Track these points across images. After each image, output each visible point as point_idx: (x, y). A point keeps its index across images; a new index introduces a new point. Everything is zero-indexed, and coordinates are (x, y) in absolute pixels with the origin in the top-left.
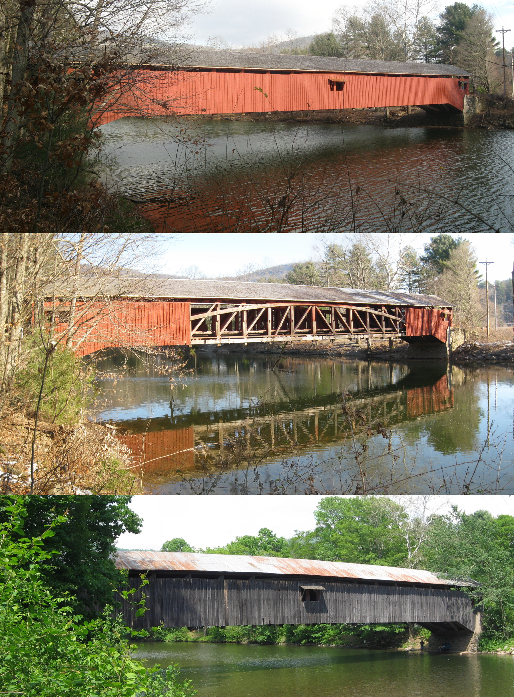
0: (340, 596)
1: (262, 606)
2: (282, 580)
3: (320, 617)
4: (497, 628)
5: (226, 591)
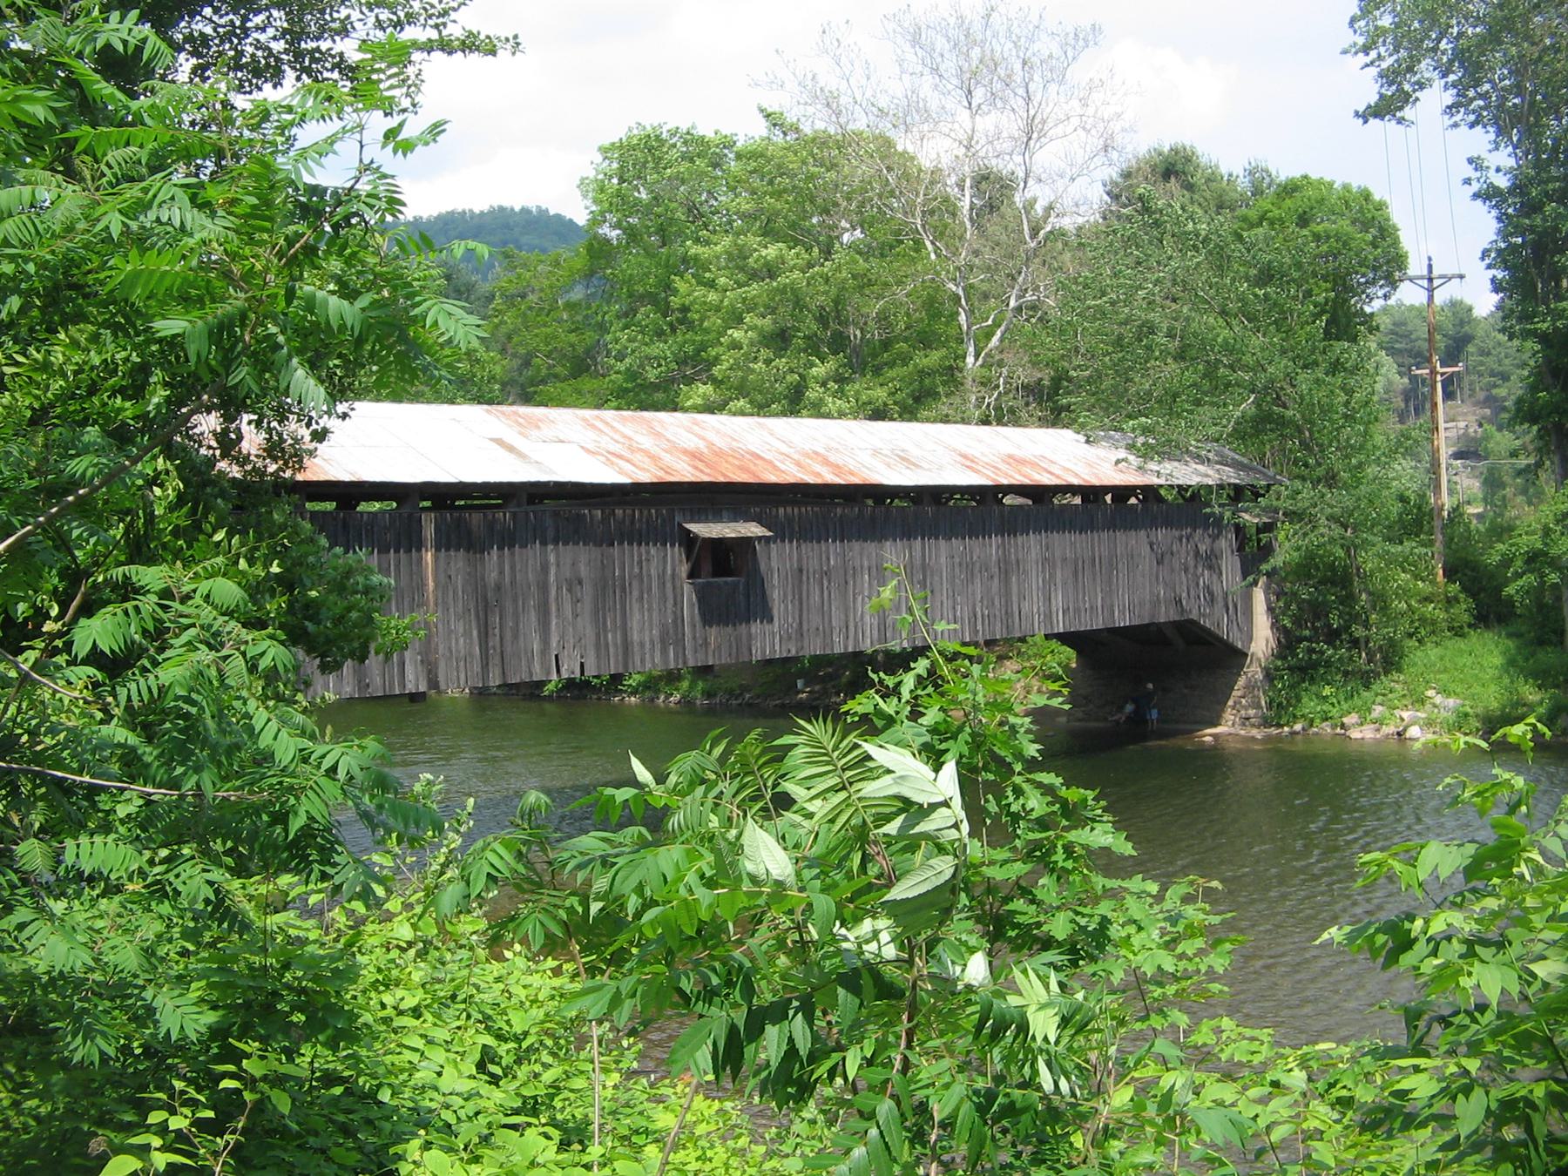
0: (813, 554)
1: (553, 608)
2: (621, 504)
3: (750, 635)
4: (1332, 637)
5: (429, 557)
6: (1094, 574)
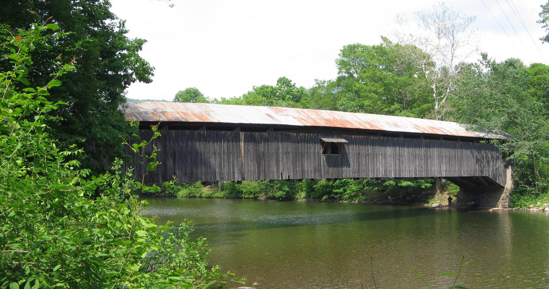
0: (363, 149)
1: (281, 159)
2: (301, 132)
3: (342, 171)
4: (529, 183)
5: (242, 144)
6: (455, 161)
